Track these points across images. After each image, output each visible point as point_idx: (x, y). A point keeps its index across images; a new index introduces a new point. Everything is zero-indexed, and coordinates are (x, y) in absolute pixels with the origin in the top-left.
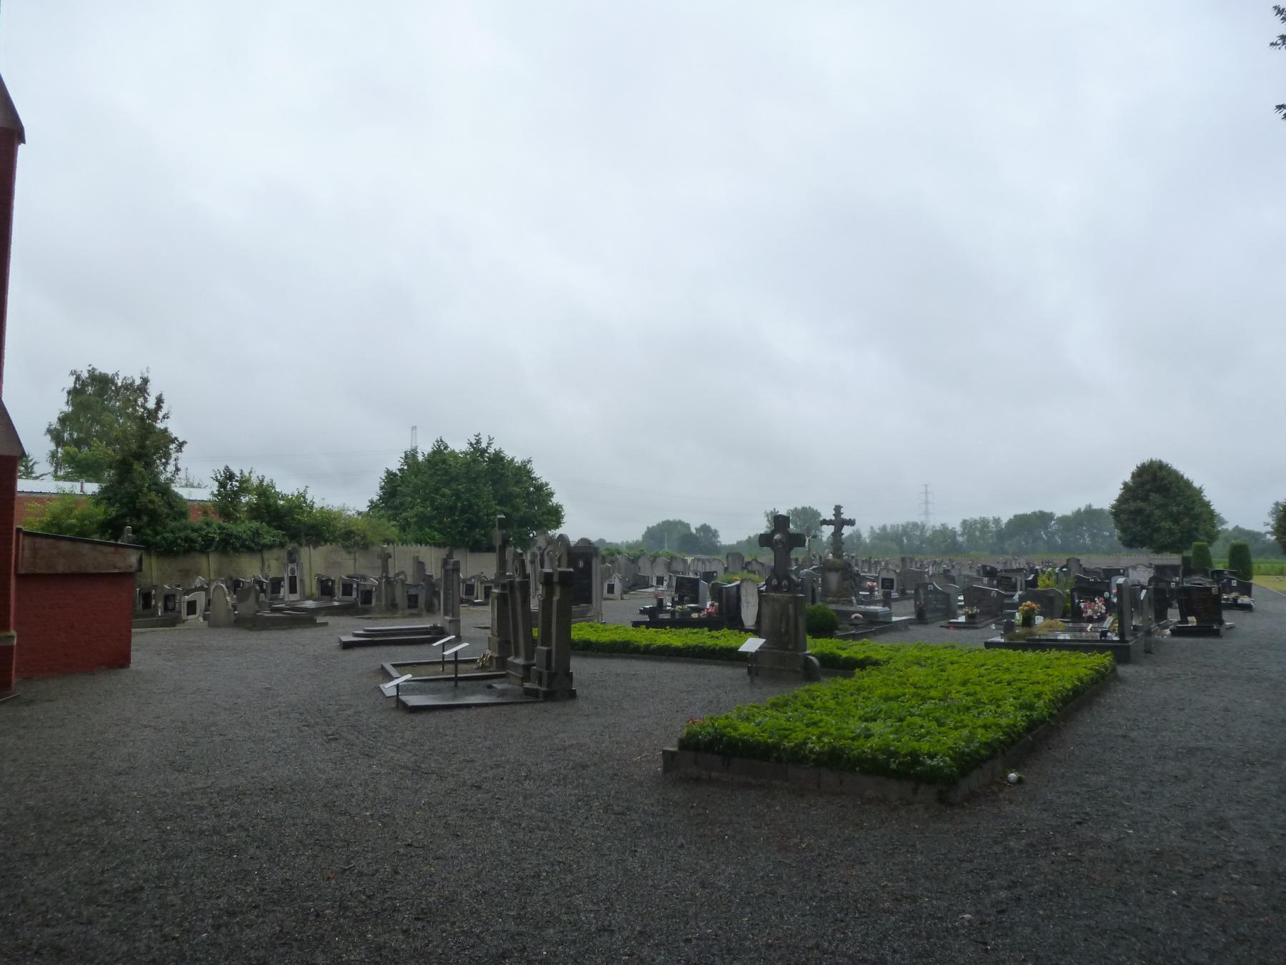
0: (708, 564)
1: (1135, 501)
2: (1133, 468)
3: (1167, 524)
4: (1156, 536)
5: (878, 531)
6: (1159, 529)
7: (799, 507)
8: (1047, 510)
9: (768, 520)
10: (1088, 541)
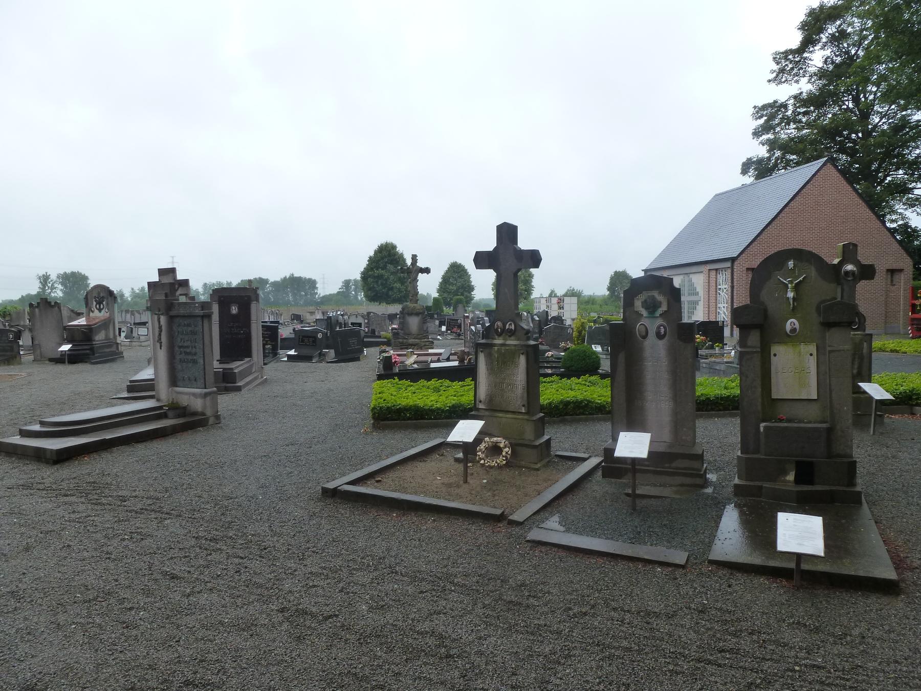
0: (137, 315)
1: (377, 269)
2: (376, 247)
3: (398, 285)
4: (390, 293)
5: (137, 291)
6: (392, 289)
7: (68, 271)
8: (264, 277)
9: (41, 282)
10: (291, 298)
